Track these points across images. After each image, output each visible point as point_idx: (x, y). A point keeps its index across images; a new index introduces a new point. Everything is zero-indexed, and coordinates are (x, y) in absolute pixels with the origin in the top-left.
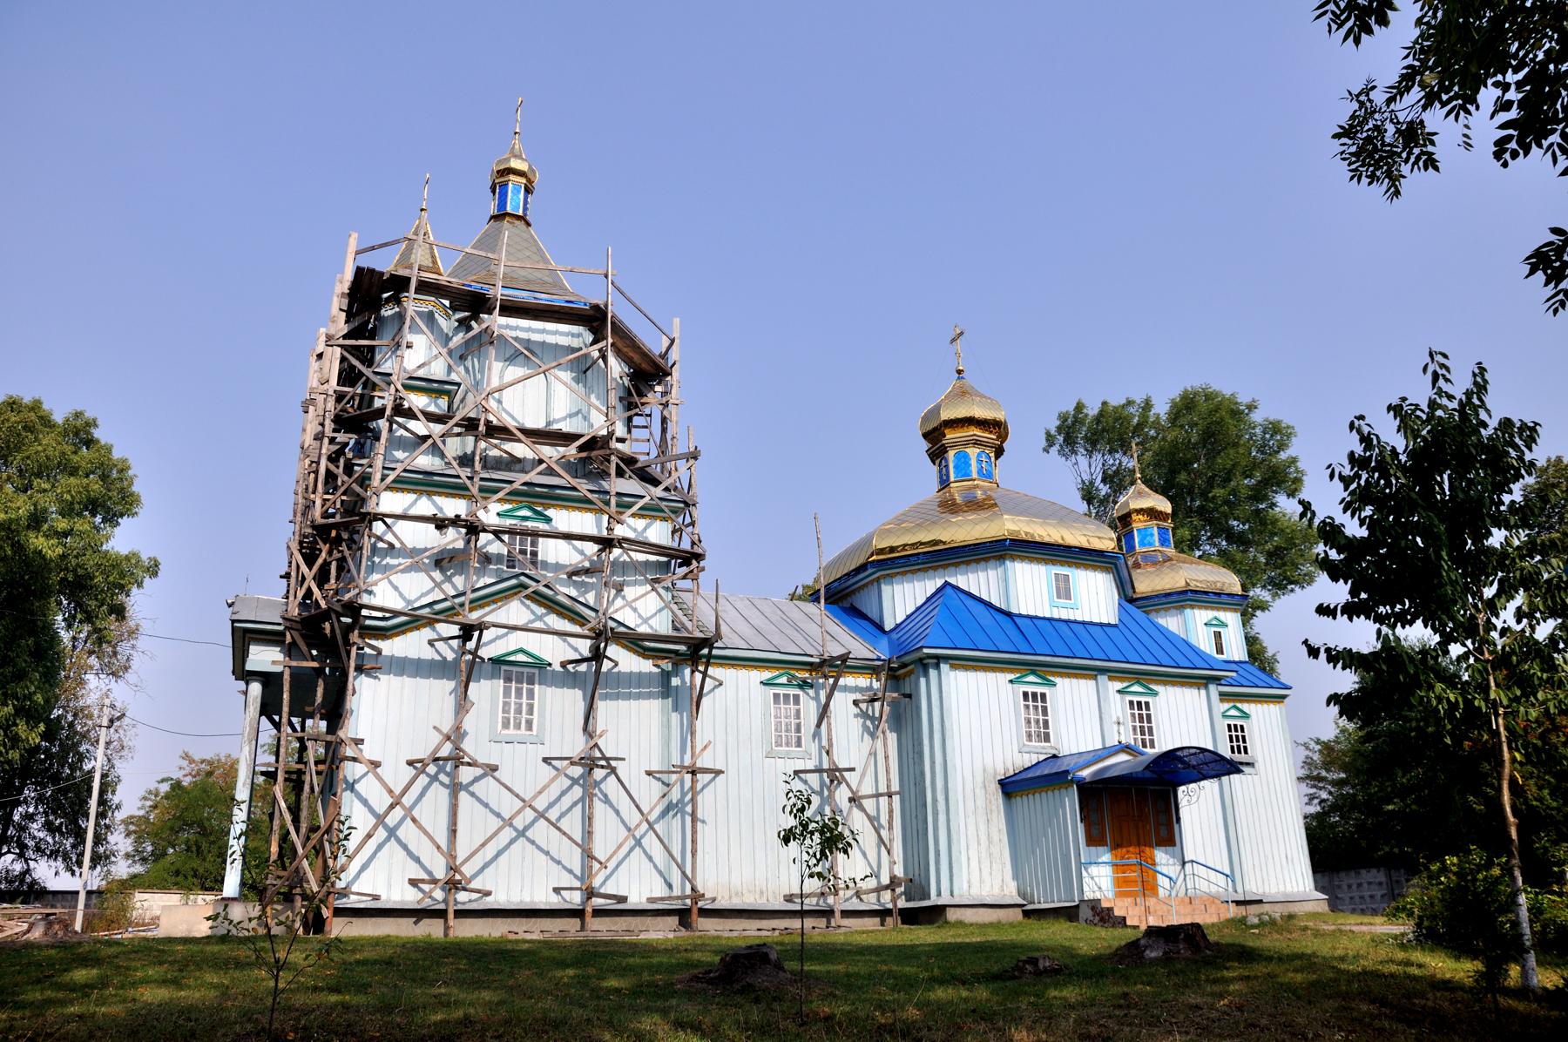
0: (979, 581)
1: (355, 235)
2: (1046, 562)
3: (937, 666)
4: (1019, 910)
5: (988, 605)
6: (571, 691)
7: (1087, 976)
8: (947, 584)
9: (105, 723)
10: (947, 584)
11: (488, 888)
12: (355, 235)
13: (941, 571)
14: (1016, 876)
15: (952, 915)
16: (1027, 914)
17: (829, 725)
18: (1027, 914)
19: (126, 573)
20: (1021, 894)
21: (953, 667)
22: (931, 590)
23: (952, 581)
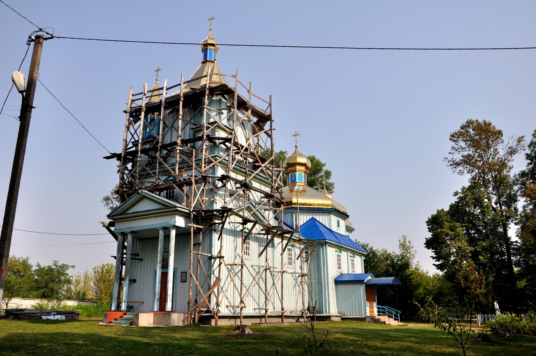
0: (321, 218)
1: (166, 81)
2: (337, 216)
3: (325, 245)
4: (340, 318)
5: (325, 226)
6: (231, 237)
7: (387, 350)
8: (313, 218)
9: (472, 329)
10: (313, 218)
11: (137, 253)
12: (166, 81)
13: (311, 214)
14: (337, 308)
15: (332, 318)
16: (342, 319)
17: (221, 239)
18: (342, 319)
19: (332, 185)
20: (338, 313)
21: (329, 246)
22: (308, 219)
23: (315, 217)
